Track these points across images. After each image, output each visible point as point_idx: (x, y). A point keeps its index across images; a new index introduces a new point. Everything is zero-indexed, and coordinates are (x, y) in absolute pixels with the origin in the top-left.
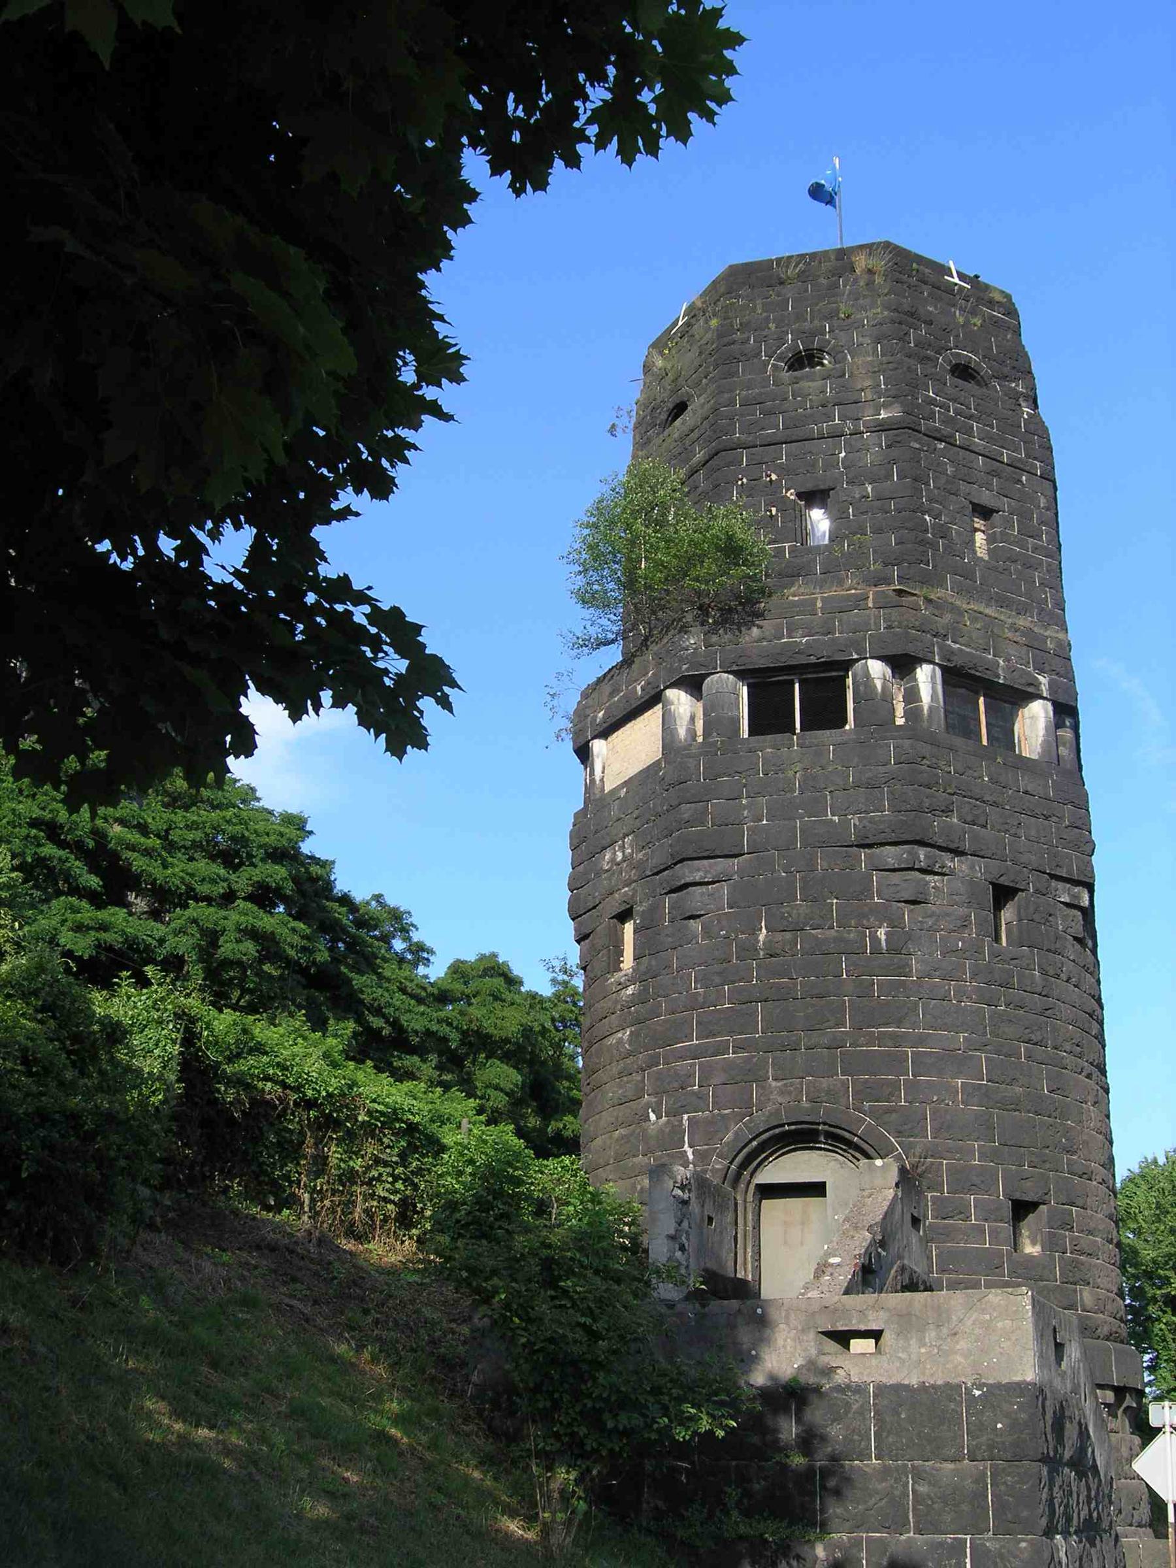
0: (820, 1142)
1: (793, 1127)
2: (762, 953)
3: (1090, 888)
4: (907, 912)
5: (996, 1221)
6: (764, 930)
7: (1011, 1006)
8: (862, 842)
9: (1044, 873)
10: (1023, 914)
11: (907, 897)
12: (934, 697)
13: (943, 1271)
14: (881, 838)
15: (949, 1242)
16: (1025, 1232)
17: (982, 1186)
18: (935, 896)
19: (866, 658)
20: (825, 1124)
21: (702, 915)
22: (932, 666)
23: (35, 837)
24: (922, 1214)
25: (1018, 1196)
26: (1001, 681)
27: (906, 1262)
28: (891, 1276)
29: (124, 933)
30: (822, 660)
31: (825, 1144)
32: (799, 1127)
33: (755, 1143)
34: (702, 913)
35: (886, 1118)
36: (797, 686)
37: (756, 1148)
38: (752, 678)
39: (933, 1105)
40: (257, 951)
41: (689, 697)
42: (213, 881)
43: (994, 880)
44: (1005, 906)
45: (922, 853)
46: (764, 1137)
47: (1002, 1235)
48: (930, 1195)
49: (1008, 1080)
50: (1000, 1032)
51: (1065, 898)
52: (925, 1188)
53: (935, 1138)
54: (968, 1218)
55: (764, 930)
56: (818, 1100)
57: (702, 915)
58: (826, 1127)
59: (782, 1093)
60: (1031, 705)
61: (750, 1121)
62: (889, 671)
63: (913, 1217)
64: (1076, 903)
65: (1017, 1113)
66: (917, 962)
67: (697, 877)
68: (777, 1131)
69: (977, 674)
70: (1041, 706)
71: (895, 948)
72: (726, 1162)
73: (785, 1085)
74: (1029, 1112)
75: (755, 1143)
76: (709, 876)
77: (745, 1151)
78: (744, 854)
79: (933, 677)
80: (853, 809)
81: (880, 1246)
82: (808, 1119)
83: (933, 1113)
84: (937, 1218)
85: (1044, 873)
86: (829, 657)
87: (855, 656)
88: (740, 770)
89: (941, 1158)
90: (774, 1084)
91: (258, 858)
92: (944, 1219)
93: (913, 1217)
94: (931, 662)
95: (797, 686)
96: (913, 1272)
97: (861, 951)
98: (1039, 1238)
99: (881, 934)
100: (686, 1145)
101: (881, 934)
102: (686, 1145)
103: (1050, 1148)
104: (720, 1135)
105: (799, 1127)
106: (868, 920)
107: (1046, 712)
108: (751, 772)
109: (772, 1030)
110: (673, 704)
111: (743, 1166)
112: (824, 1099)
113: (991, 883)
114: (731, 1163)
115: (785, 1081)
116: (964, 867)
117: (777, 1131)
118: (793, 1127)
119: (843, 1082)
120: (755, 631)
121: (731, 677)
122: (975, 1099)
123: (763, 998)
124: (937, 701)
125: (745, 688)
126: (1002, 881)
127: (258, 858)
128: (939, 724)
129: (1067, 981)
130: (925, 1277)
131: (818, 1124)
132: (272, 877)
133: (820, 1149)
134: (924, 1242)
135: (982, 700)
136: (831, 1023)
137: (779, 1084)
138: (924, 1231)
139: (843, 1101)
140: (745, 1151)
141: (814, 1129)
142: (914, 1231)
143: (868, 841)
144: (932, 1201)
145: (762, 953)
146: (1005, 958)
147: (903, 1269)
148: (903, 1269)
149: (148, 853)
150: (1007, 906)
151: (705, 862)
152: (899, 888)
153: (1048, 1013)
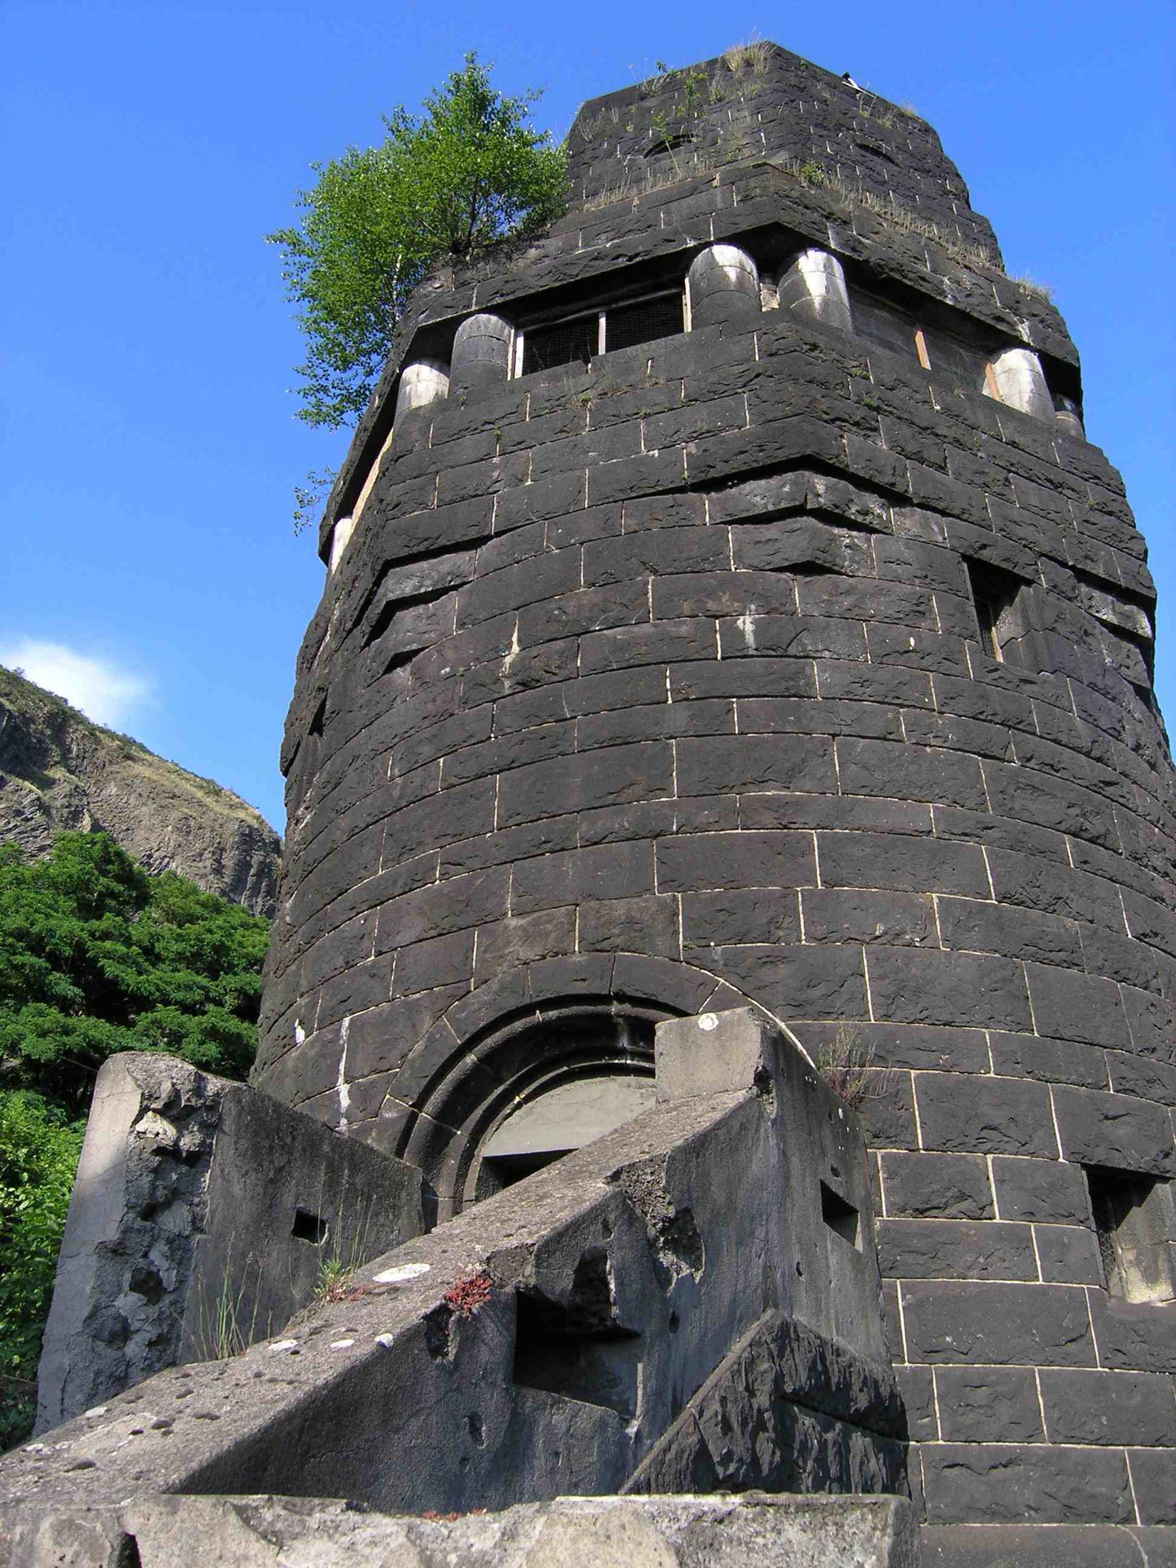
0: (622, 1053)
1: (553, 1014)
2: (507, 684)
3: (1148, 605)
4: (798, 590)
5: (1055, 1217)
6: (516, 648)
7: (1032, 764)
8: (702, 476)
9: (1064, 564)
10: (1034, 620)
11: (796, 557)
12: (830, 287)
13: (929, 1353)
14: (739, 464)
15: (938, 1272)
16: (1125, 1254)
17: (1013, 1131)
18: (852, 561)
19: (709, 244)
20: (622, 998)
21: (416, 652)
22: (825, 254)
23: (11, 945)
24: (860, 1192)
25: (1100, 1156)
26: (949, 302)
27: (801, 1317)
28: (731, 1357)
29: (86, 1036)
30: (638, 259)
31: (633, 1055)
32: (565, 1011)
33: (471, 1059)
34: (414, 647)
35: (767, 974)
36: (603, 321)
37: (477, 1069)
38: (533, 323)
39: (874, 946)
40: (220, 1053)
41: (435, 372)
42: (188, 988)
43: (970, 552)
44: (996, 618)
45: (821, 483)
46: (490, 1041)
47: (1073, 1257)
48: (880, 1153)
49: (1045, 899)
50: (1017, 807)
51: (1108, 615)
52: (866, 1137)
53: (887, 1016)
54: (982, 1212)
55: (516, 648)
56: (605, 945)
57: (416, 652)
58: (627, 1008)
59: (528, 937)
60: (1003, 356)
61: (461, 1009)
62: (750, 265)
63: (827, 1195)
64: (1129, 626)
65: (1074, 971)
66: (822, 670)
67: (408, 588)
68: (519, 1025)
69: (906, 281)
70: (1021, 358)
71: (770, 648)
72: (406, 1105)
73: (536, 923)
74: (1100, 970)
75: (471, 1059)
76: (428, 582)
77: (452, 1076)
78: (489, 538)
79: (828, 268)
80: (683, 434)
81: (672, 1245)
82: (580, 988)
83: (876, 961)
84: (903, 1210)
85: (1064, 564)
86: (647, 252)
87: (691, 244)
88: (492, 418)
89: (904, 1063)
90: (513, 922)
91: (241, 967)
92: (921, 1212)
93: (827, 1195)
94: (823, 247)
95: (603, 321)
96: (822, 1353)
97: (705, 654)
98: (1162, 1265)
99: (746, 624)
100: (341, 1079)
101: (746, 624)
102: (341, 1079)
103: (1159, 1054)
104: (402, 1046)
105: (565, 1011)
106: (719, 599)
107: (1031, 364)
108: (512, 418)
109: (518, 819)
110: (409, 383)
111: (451, 1114)
112: (618, 941)
113: (966, 558)
114: (420, 1104)
115: (535, 915)
116: (908, 523)
117: (519, 1025)
118: (553, 1014)
119: (661, 904)
120: (533, 253)
121: (494, 318)
122: (975, 1272)
123: (504, 763)
124: (837, 291)
125: (521, 341)
126: (985, 555)
127: (241, 967)
128: (843, 318)
129: (1133, 750)
130: (877, 1370)
131: (605, 999)
132: (250, 984)
133: (625, 1070)
134: (869, 1276)
135: (919, 338)
136: (637, 790)
137: (522, 922)
138: (869, 1241)
139: (661, 943)
140: (452, 1076)
141: (599, 1016)
142: (830, 1234)
143: (713, 474)
144: (887, 1170)
145: (507, 684)
146: (1009, 677)
147: (785, 1335)
148: (785, 1335)
149: (123, 960)
150: (1003, 614)
151: (424, 565)
152: (778, 545)
153: (1109, 790)
